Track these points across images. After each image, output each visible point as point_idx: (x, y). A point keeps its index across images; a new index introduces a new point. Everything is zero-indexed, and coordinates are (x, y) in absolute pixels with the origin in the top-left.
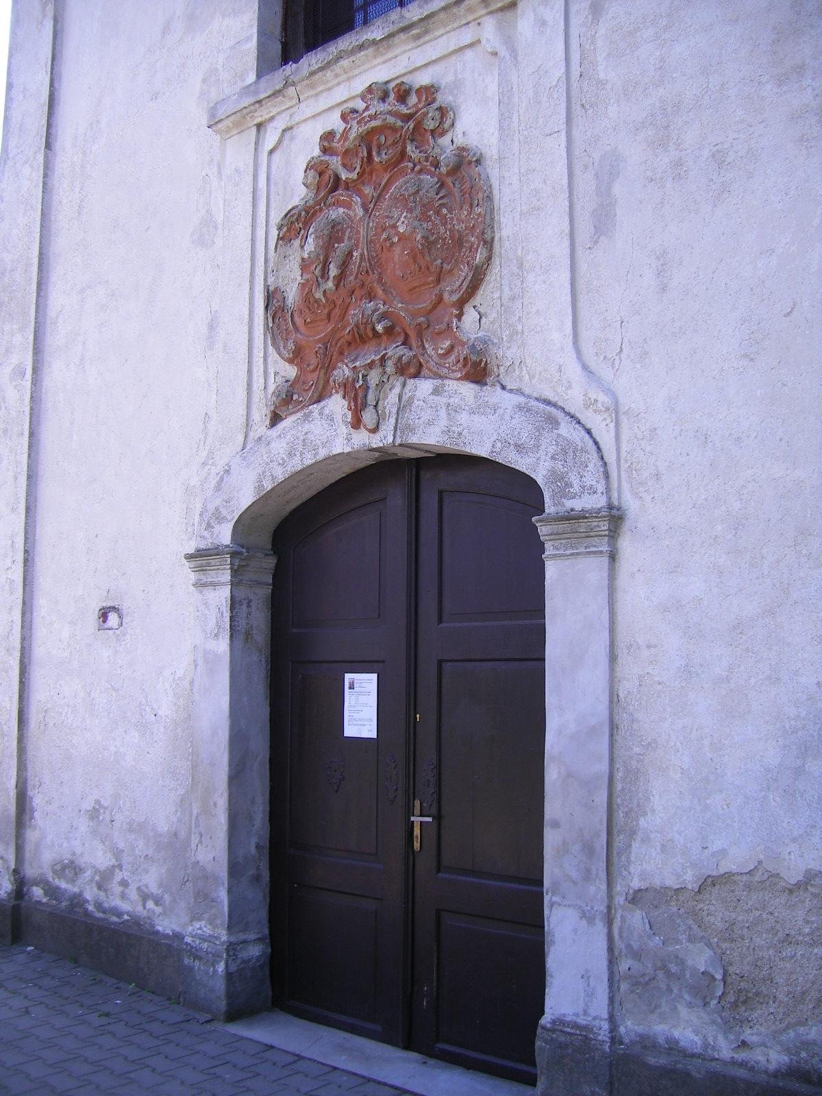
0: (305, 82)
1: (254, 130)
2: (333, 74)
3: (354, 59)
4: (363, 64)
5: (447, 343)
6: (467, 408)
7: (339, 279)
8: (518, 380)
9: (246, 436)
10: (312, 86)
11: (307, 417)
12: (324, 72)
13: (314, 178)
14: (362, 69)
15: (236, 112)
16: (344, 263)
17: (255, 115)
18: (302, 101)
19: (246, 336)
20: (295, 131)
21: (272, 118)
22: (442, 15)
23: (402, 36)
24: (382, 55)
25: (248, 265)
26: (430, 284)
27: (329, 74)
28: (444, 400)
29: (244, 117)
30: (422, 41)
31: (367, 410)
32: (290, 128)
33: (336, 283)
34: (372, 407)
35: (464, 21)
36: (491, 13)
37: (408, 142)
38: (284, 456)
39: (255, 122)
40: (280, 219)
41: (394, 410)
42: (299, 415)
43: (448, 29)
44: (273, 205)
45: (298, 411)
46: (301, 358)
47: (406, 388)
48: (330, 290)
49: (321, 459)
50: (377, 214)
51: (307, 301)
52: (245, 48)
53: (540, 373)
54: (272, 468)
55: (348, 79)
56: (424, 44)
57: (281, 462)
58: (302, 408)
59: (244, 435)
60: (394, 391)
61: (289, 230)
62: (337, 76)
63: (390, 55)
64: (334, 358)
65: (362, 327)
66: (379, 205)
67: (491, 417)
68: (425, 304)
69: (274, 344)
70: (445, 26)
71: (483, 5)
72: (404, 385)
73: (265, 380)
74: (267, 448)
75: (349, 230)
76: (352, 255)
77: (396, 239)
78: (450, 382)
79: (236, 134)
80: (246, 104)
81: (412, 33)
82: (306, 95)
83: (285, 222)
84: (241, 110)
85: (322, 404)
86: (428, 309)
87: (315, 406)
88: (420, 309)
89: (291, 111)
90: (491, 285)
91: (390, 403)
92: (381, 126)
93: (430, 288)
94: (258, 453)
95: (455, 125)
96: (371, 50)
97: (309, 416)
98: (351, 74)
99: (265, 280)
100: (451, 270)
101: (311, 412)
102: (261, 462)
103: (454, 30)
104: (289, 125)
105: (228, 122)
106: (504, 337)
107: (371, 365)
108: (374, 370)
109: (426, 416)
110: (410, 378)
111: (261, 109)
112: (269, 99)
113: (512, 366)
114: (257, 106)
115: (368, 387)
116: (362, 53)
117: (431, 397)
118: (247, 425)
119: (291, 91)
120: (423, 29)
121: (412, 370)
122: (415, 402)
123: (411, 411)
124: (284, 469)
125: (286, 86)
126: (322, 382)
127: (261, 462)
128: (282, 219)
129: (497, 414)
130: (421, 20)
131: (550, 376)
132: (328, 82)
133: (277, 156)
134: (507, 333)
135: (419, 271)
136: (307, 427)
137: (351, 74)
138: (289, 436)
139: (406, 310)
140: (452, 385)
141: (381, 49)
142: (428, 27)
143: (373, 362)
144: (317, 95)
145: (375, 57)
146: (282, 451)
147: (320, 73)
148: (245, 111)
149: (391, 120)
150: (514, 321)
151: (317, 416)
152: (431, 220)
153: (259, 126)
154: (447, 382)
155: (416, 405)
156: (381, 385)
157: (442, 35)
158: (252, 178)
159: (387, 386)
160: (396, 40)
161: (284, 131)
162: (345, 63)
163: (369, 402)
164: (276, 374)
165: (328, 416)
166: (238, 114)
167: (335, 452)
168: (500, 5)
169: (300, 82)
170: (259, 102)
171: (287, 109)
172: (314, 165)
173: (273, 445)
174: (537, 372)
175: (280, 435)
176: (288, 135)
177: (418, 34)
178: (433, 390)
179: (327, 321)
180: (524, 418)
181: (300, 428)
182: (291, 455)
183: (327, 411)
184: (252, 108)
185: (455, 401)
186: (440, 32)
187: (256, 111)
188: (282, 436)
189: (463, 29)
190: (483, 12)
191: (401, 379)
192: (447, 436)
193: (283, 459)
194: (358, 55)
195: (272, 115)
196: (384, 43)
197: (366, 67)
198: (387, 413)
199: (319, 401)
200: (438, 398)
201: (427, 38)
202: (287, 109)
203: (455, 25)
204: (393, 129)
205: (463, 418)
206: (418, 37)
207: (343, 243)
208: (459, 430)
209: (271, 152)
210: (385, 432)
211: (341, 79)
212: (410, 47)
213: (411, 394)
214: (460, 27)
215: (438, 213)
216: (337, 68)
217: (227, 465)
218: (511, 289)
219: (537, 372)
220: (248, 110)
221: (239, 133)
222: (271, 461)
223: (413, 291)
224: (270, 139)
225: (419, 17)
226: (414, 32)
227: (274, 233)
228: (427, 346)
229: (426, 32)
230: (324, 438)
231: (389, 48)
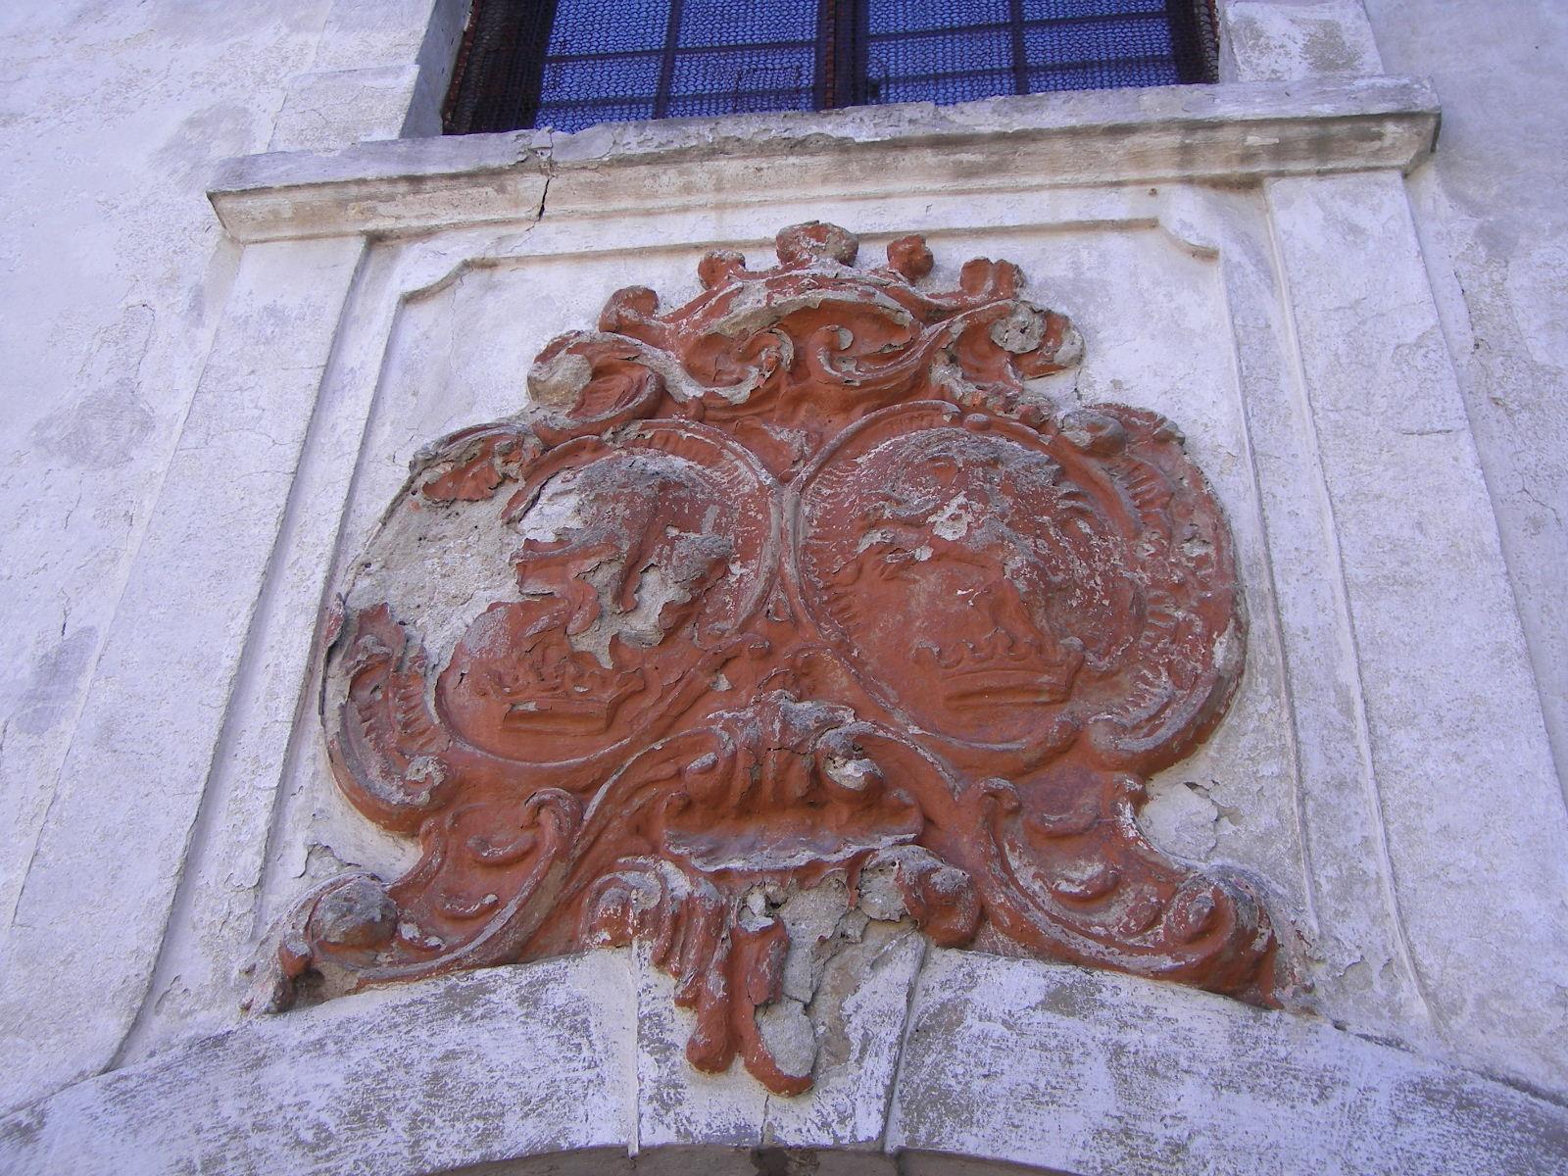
0: (585, 176)
1: (357, 246)
2: (680, 181)
3: (764, 165)
4: (780, 185)
5: (1093, 869)
6: (1197, 1066)
7: (679, 617)
8: (1385, 1012)
9: (136, 1025)
10: (600, 192)
11: (458, 1004)
12: (654, 169)
13: (577, 376)
14: (770, 195)
15: (325, 184)
16: (701, 580)
17: (382, 208)
18: (549, 218)
19: (216, 717)
20: (499, 274)
21: (428, 233)
22: (1060, 145)
23: (929, 157)
24: (850, 180)
25: (270, 531)
26: (1038, 692)
27: (670, 177)
28: (1100, 1032)
29: (342, 204)
30: (975, 183)
31: (780, 1011)
32: (487, 265)
33: (670, 622)
34: (800, 1006)
35: (1110, 177)
36: (1189, 181)
37: (942, 357)
38: (324, 1117)
39: (371, 226)
40: (437, 437)
41: (888, 1034)
42: (421, 989)
43: (1059, 179)
44: (389, 412)
45: (422, 976)
46: (457, 818)
47: (927, 974)
48: (639, 638)
49: (512, 1154)
50: (826, 491)
51: (538, 652)
52: (368, 84)
53: (1481, 1001)
54: (260, 1152)
55: (720, 207)
56: (980, 191)
57: (308, 1136)
58: (445, 969)
59: (126, 1019)
60: (885, 973)
61: (458, 475)
62: (687, 189)
63: (869, 188)
64: (609, 837)
65: (772, 761)
66: (830, 473)
67: (1309, 1107)
68: (1021, 740)
69: (342, 756)
70: (1055, 171)
71: (1178, 159)
72: (923, 964)
73: (266, 860)
74: (250, 1077)
75: (716, 509)
76: (727, 571)
77: (924, 554)
78: (1123, 981)
79: (290, 239)
80: (371, 173)
81: (957, 156)
82: (569, 207)
83: (454, 450)
84: (346, 183)
85: (538, 970)
86: (1026, 757)
87: (504, 971)
88: (994, 752)
89: (503, 231)
90: (1246, 742)
91: (867, 1006)
92: (852, 305)
93: (1035, 704)
94: (194, 1088)
95: (1085, 362)
96: (822, 161)
97: (471, 1000)
98: (733, 198)
99: (330, 580)
100: (1107, 675)
101: (482, 989)
102: (207, 1124)
103: (1075, 186)
104: (491, 254)
105: (285, 203)
106: (1323, 881)
107: (807, 875)
108: (813, 895)
109: (1020, 1070)
110: (947, 945)
111: (410, 198)
112: (449, 183)
113: (1358, 968)
114: (403, 187)
115: (787, 945)
116: (792, 160)
117: (1039, 1016)
118: (151, 989)
119: (532, 185)
120: (995, 158)
121: (961, 923)
122: (968, 1021)
123: (950, 1047)
124: (322, 1165)
125: (520, 167)
126: (547, 901)
127: (207, 1124)
128: (441, 443)
129: (1333, 1103)
130: (1000, 137)
131: (1524, 1015)
132: (654, 195)
133: (423, 315)
134: (1331, 871)
135: (1010, 649)
136: (455, 1033)
137: (733, 198)
138: (360, 1054)
139: (939, 749)
140: (1126, 990)
141: (854, 167)
142: (1010, 157)
143: (814, 867)
144: (603, 216)
145: (825, 180)
146: (318, 1099)
147: (642, 168)
148: (354, 190)
149: (880, 298)
150: (1350, 845)
151: (511, 1004)
152: (1045, 535)
153: (375, 240)
154: (1107, 978)
155: (975, 1031)
156: (832, 946)
157: (1039, 188)
158: (328, 338)
159: (857, 956)
160: (908, 159)
161: (467, 265)
162: (731, 167)
163: (791, 988)
164: (316, 850)
165: (561, 1015)
166: (329, 192)
167: (580, 1139)
168: (1219, 171)
169: (569, 169)
170: (415, 181)
171: (495, 223)
172: (589, 345)
173: (278, 1072)
174: (1470, 998)
175: (320, 1044)
176: (474, 279)
177: (973, 164)
178: (1048, 995)
179: (601, 724)
180: (1453, 1127)
181: (424, 1034)
182: (360, 1117)
183: (557, 996)
184: (385, 188)
185: (1148, 1039)
186: (1037, 180)
187: (391, 198)
188: (331, 1047)
189: (1102, 191)
190: (1173, 173)
191: (916, 941)
192: (1120, 1150)
193: (320, 1127)
194: (779, 161)
195: (433, 222)
196: (870, 157)
197: (787, 193)
198: (855, 1038)
199: (521, 954)
200: (1066, 1022)
201: (993, 182)
202: (495, 223)
203: (1084, 178)
204: (885, 322)
205: (1190, 1098)
206: (971, 172)
207: (698, 530)
208: (1174, 1133)
209: (411, 299)
210: (841, 1099)
211: (694, 199)
212: (938, 186)
213: (948, 994)
214: (1095, 185)
215: (1063, 525)
216: (701, 173)
217: (30, 1106)
218: (1330, 761)
219: (1470, 998)
220: (365, 190)
221: (302, 238)
222: (259, 1127)
223: (970, 701)
224: (415, 268)
225: (997, 129)
226: (967, 157)
227: (389, 477)
228: (1014, 864)
229: (998, 168)
230: (535, 1085)
231: (880, 169)
